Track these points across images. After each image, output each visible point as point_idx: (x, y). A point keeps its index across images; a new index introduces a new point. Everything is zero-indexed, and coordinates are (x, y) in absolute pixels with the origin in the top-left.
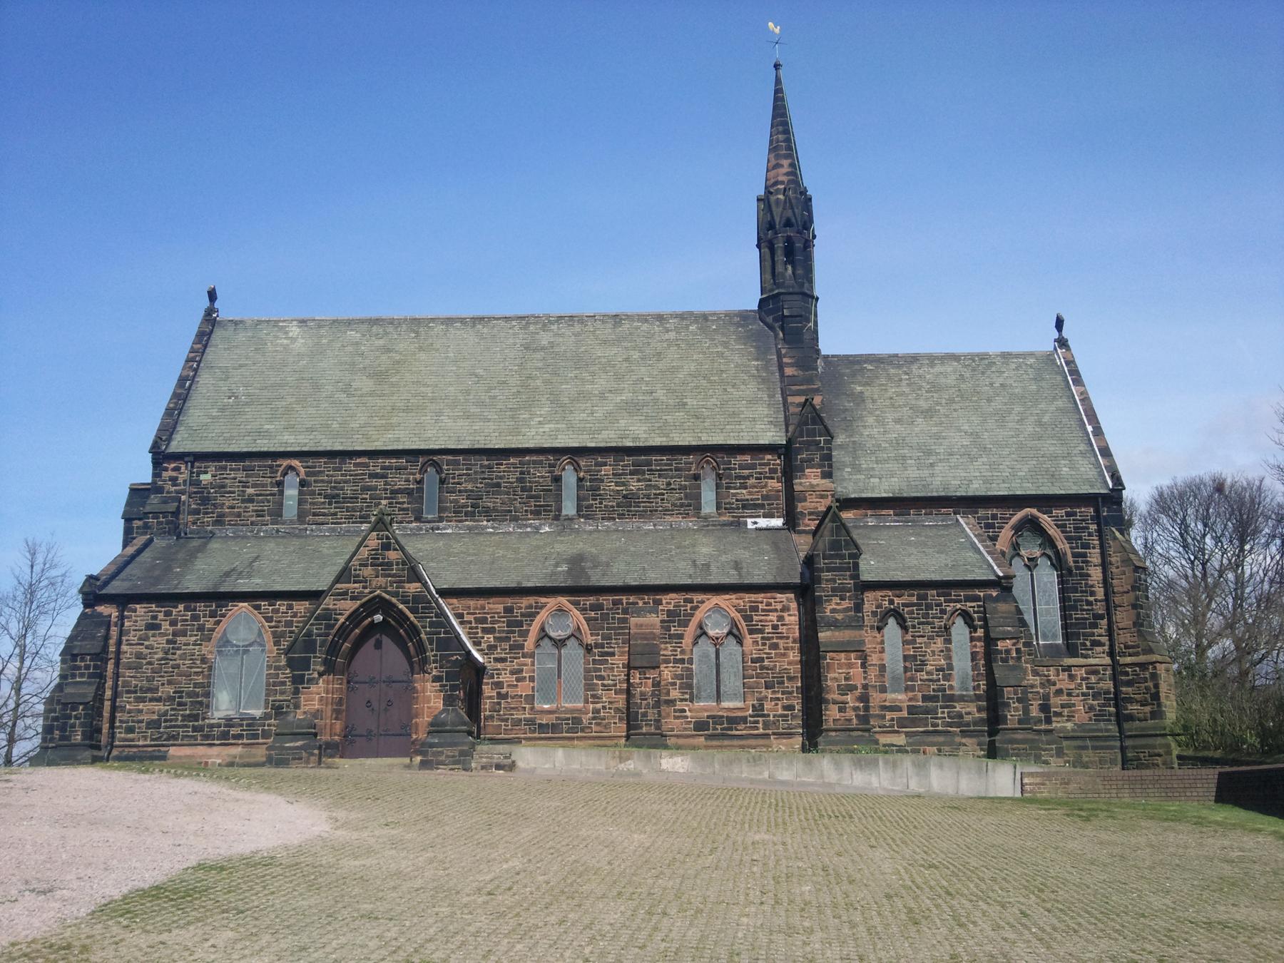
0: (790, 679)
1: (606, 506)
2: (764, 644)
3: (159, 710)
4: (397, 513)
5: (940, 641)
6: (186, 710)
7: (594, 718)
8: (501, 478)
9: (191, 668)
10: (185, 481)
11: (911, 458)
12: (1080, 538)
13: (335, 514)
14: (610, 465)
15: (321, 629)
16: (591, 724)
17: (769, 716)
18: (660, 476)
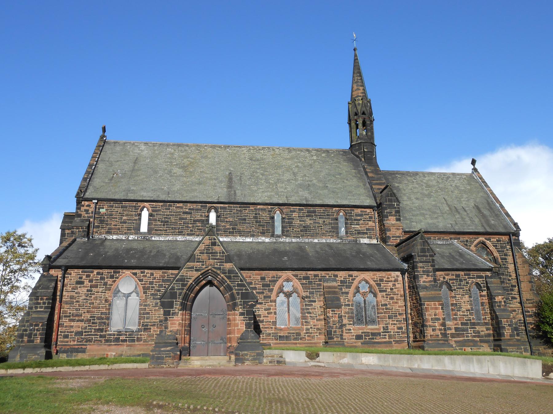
0: (400, 314)
1: (295, 231)
4: (196, 231)
5: (467, 296)
6: (97, 326)
7: (307, 333)
8: (246, 216)
9: (100, 304)
10: (92, 212)
14: (297, 212)
15: (180, 286)
16: (305, 336)
17: (391, 332)
18: (320, 218)
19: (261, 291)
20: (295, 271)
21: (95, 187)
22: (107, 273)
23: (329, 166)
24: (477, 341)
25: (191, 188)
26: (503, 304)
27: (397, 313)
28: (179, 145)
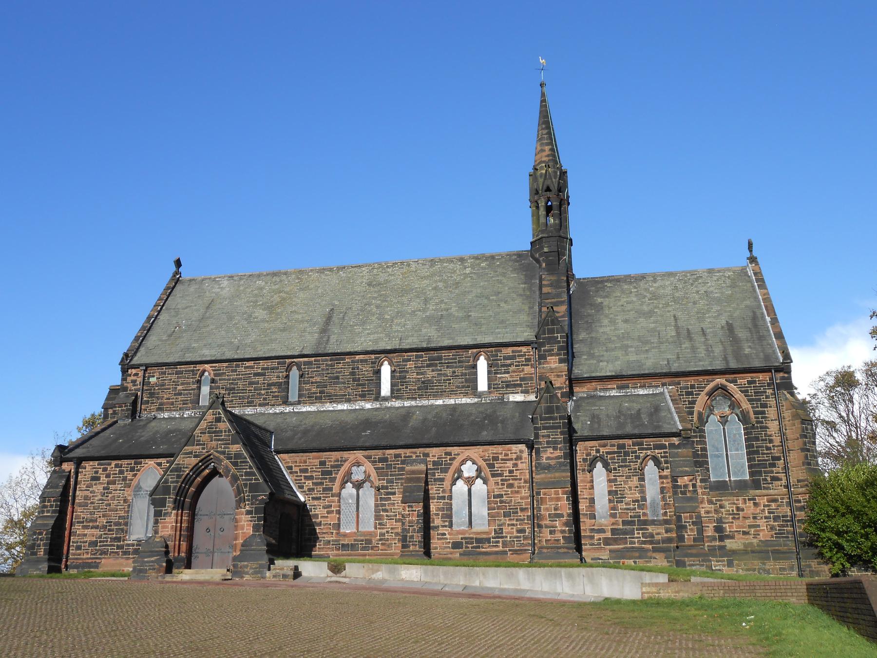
0: (522, 510)
1: (410, 390)
2: (503, 484)
3: (97, 534)
4: (271, 399)
5: (636, 478)
6: (113, 534)
7: (380, 540)
8: (339, 372)
9: (118, 505)
11: (631, 347)
12: (760, 400)
13: (232, 401)
14: (413, 361)
16: (379, 544)
17: (506, 537)
18: (448, 367)
19: (320, 481)
20: (367, 450)
21: (148, 348)
22: (127, 464)
23: (485, 281)
24: (648, 550)
25: (270, 338)
26: (691, 489)
27: (517, 508)
28: (274, 274)
